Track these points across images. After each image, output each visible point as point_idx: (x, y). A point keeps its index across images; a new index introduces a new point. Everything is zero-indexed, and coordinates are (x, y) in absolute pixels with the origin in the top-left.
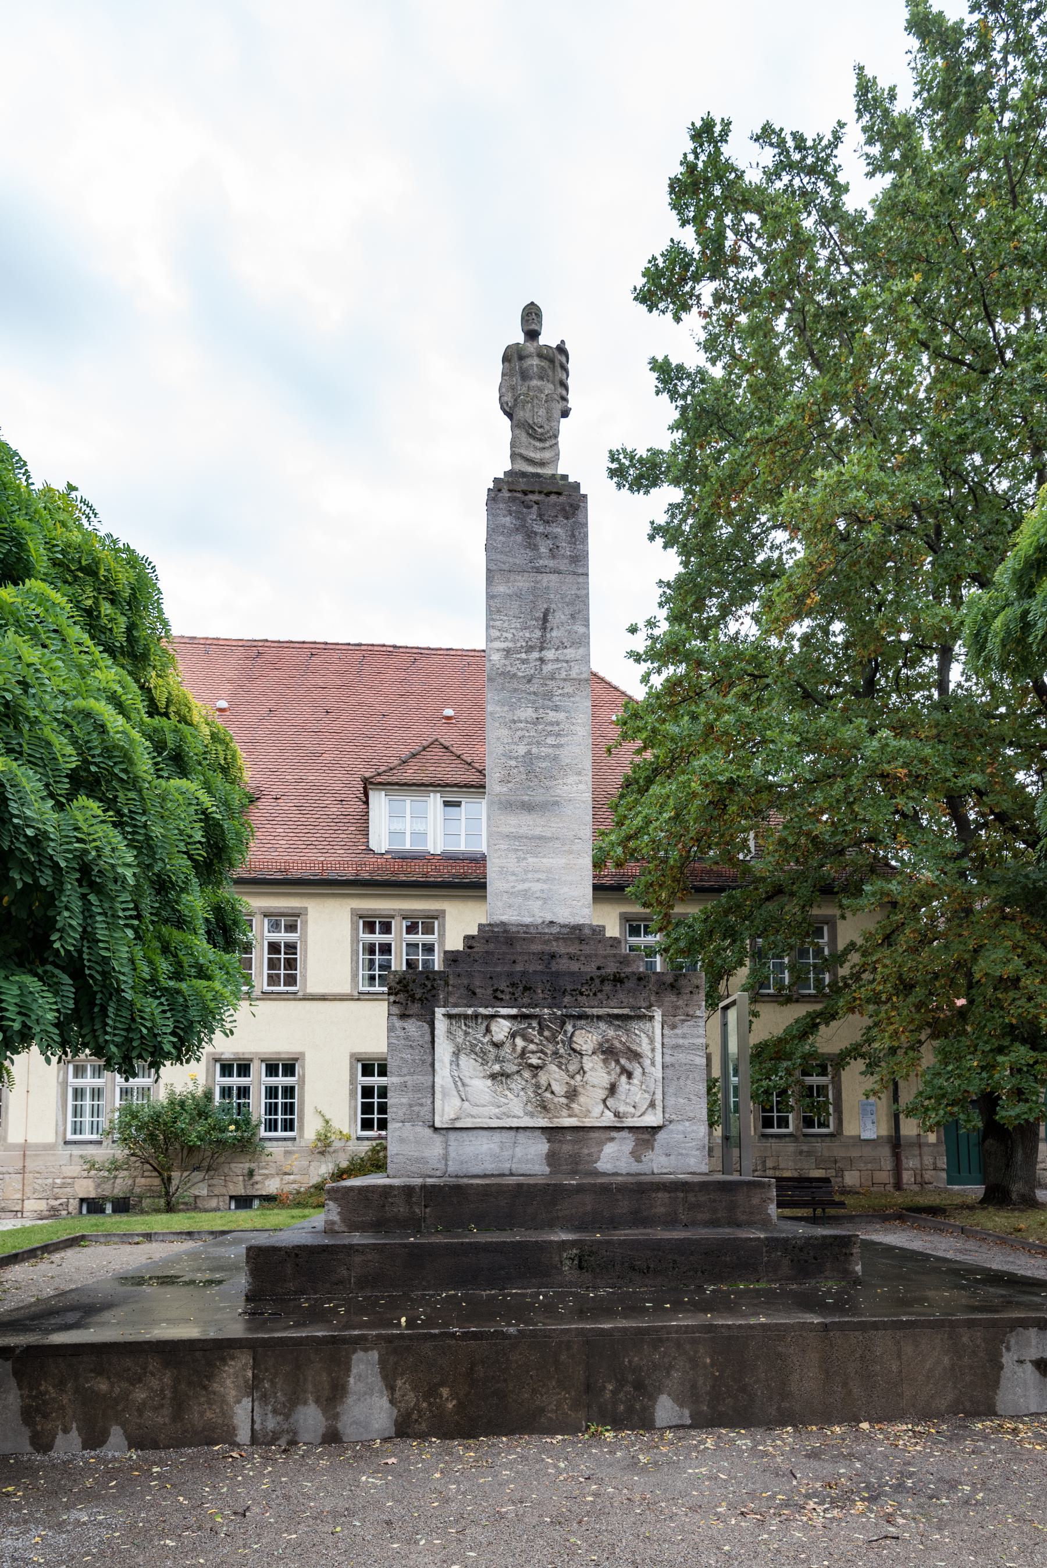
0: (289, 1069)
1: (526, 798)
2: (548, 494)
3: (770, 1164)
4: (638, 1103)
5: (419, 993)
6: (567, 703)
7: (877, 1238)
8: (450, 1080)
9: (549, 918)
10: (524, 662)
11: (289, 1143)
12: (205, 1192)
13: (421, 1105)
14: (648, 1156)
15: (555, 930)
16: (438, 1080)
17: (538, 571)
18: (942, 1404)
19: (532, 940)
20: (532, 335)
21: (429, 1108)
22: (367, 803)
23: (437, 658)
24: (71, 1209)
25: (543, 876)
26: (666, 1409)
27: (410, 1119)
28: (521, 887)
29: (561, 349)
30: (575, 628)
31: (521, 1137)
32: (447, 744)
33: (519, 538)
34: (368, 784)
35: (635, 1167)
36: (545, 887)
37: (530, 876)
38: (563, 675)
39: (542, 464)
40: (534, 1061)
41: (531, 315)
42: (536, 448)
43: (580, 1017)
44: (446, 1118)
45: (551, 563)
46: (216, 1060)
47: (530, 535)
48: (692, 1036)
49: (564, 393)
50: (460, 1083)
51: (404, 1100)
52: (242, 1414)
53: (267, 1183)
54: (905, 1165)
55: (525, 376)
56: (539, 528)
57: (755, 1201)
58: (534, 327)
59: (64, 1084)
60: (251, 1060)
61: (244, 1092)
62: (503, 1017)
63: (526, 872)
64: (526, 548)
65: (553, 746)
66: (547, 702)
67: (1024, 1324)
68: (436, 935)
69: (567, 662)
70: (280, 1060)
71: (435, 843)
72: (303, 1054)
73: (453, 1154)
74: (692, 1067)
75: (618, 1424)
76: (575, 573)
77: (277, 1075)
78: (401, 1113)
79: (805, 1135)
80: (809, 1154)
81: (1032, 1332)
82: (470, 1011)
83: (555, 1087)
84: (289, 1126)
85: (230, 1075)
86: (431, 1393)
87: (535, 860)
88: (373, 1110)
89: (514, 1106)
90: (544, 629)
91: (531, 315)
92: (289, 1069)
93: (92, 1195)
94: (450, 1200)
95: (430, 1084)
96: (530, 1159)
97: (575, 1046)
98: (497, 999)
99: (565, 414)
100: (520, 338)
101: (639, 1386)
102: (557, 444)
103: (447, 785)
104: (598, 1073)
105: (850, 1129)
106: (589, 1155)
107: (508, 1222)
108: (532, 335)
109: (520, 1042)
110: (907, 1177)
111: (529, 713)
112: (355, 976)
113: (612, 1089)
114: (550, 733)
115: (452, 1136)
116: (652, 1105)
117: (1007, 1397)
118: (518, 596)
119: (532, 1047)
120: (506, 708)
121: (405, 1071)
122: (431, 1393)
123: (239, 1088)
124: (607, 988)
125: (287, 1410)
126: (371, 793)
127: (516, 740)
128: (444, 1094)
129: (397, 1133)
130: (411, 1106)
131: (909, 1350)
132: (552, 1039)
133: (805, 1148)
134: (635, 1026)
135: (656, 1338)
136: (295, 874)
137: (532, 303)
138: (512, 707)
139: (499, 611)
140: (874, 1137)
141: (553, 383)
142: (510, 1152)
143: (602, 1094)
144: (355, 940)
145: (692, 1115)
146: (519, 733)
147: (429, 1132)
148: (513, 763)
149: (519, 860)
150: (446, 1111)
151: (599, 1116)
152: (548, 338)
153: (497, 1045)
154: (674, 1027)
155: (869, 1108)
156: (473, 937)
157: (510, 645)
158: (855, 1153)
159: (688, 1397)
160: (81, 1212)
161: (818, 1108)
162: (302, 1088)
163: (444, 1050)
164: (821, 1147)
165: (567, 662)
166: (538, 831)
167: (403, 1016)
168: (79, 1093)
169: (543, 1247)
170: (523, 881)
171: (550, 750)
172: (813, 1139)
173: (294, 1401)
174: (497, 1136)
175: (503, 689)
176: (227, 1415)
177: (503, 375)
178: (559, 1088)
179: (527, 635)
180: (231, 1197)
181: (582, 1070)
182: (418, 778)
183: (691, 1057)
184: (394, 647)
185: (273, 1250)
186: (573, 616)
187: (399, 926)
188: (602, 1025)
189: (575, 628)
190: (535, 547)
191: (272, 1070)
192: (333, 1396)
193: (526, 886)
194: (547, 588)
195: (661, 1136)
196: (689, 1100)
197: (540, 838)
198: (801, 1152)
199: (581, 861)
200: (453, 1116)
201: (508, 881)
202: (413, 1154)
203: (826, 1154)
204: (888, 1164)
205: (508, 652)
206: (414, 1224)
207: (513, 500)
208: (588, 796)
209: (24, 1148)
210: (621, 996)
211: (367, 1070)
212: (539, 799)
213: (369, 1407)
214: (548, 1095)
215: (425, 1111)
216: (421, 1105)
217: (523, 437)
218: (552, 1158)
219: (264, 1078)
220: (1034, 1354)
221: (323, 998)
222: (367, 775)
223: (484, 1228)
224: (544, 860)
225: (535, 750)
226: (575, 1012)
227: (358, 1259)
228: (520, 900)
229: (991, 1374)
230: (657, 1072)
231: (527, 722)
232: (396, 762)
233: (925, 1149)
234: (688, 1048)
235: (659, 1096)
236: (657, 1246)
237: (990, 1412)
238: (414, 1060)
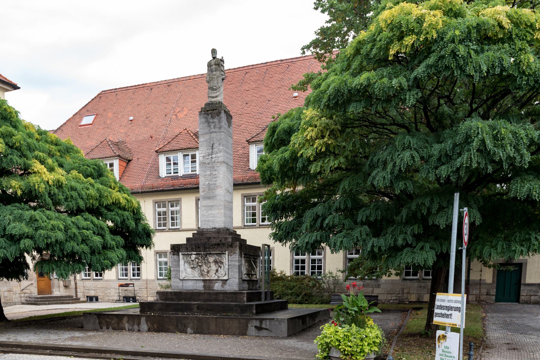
3: (405, 291)
4: (222, 274)
5: (176, 249)
9: (214, 227)
10: (208, 159)
14: (225, 286)
15: (214, 230)
17: (211, 133)
18: (237, 333)
19: (207, 234)
26: (189, 330)
27: (175, 278)
28: (207, 219)
29: (222, 60)
31: (198, 281)
33: (206, 124)
35: (222, 289)
40: (200, 264)
41: (214, 51)
43: (210, 254)
45: (214, 130)
47: (209, 123)
50: (185, 270)
52: (127, 326)
56: (211, 121)
57: (241, 297)
59: (156, 260)
67: (253, 319)
74: (235, 265)
75: (181, 332)
79: (424, 279)
81: (254, 321)
83: (205, 270)
86: (153, 325)
89: (196, 275)
90: (212, 149)
91: (214, 51)
94: (179, 295)
96: (199, 286)
98: (192, 250)
101: (185, 326)
104: (214, 267)
107: (190, 300)
108: (214, 58)
109: (197, 260)
111: (208, 173)
113: (217, 271)
114: (214, 178)
116: (226, 274)
117: (249, 332)
118: (206, 141)
122: (153, 325)
124: (216, 247)
125: (133, 325)
128: (182, 272)
131: (231, 323)
132: (204, 259)
133: (423, 285)
134: (222, 256)
135: (187, 318)
138: (205, 171)
143: (215, 272)
149: (207, 212)
150: (182, 276)
151: (213, 277)
152: (219, 56)
153: (193, 261)
154: (231, 256)
159: (193, 328)
163: (182, 262)
166: (211, 204)
167: (174, 255)
168: (160, 263)
169: (190, 304)
173: (134, 324)
174: (193, 281)
176: (125, 326)
178: (205, 271)
181: (210, 266)
184: (281, 60)
185: (143, 303)
188: (215, 256)
190: (210, 126)
192: (139, 324)
195: (228, 282)
197: (212, 206)
198: (421, 287)
202: (176, 285)
205: (204, 157)
206: (172, 300)
207: (205, 113)
209: (147, 280)
210: (219, 248)
212: (212, 195)
213: (144, 326)
217: (210, 91)
218: (204, 286)
220: (254, 325)
223: (185, 300)
226: (208, 253)
227: (158, 305)
229: (246, 328)
230: (227, 267)
232: (261, 130)
233: (483, 286)
235: (227, 272)
236: (212, 305)
237: (246, 335)
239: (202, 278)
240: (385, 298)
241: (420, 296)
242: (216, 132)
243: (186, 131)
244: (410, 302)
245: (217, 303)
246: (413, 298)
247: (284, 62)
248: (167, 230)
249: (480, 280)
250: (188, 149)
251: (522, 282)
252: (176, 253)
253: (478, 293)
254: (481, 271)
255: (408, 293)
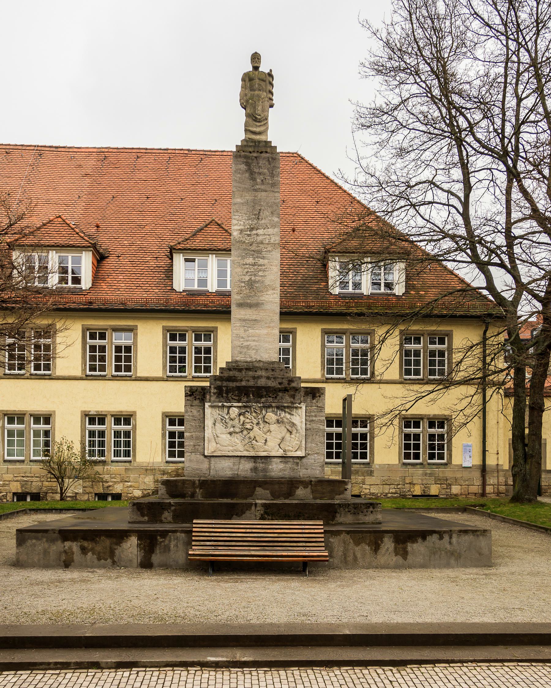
0: (127, 421)
1: (249, 301)
2: (261, 152)
6: (268, 255)
7: (427, 515)
8: (212, 434)
9: (259, 359)
10: (249, 235)
11: (128, 464)
12: (81, 491)
13: (199, 445)
16: (206, 435)
17: (256, 190)
20: (256, 68)
21: (202, 447)
22: (172, 259)
23: (215, 158)
24: (8, 498)
25: (256, 339)
27: (194, 451)
28: (246, 344)
29: (270, 75)
30: (273, 218)
32: (219, 222)
34: (172, 251)
36: (257, 344)
37: (250, 338)
38: (267, 241)
39: (260, 133)
40: (248, 426)
41: (256, 58)
42: (257, 126)
44: (210, 452)
45: (263, 187)
46: (86, 415)
48: (319, 416)
49: (271, 96)
51: (192, 443)
53: (116, 486)
54: (488, 483)
55: (252, 89)
58: (256, 65)
60: (106, 415)
61: (102, 434)
62: (235, 407)
63: (248, 337)
64: (250, 180)
65: (262, 276)
66: (259, 255)
68: (212, 342)
69: (269, 235)
70: (122, 415)
71: (212, 285)
72: (135, 412)
73: (212, 467)
76: (273, 191)
77: (121, 425)
78: (190, 449)
79: (429, 464)
80: (431, 475)
82: (220, 404)
84: (127, 454)
85: (94, 424)
87: (253, 331)
88: (175, 444)
91: (256, 58)
92: (127, 421)
93: (20, 491)
95: (203, 436)
96: (245, 469)
97: (266, 420)
99: (272, 106)
100: (250, 69)
102: (267, 123)
103: (220, 250)
105: (456, 461)
106: (272, 469)
108: (256, 68)
110: (489, 489)
112: (164, 366)
115: (212, 459)
118: (247, 203)
119: (248, 421)
120: (240, 258)
121: (192, 430)
123: (99, 431)
126: (174, 255)
127: (245, 273)
129: (189, 458)
130: (194, 446)
134: (294, 412)
136: (130, 305)
137: (256, 53)
138: (243, 258)
139: (237, 211)
140: (470, 465)
141: (266, 92)
142: (237, 467)
144: (165, 344)
145: (318, 451)
146: (246, 270)
147: (202, 457)
148: (243, 285)
150: (210, 448)
152: (264, 68)
155: (468, 448)
156: (223, 368)
157: (242, 227)
158: (458, 475)
160: (13, 501)
161: (439, 447)
162: (135, 432)
163: (209, 422)
164: (440, 472)
165: (269, 235)
166: (254, 317)
170: (247, 341)
171: (260, 278)
172: (434, 467)
174: (232, 460)
175: (239, 249)
177: (242, 87)
179: (250, 222)
180: (96, 494)
182: (202, 245)
183: (319, 425)
184: (188, 150)
186: (272, 213)
187: (190, 336)
189: (273, 218)
190: (253, 179)
191: (118, 421)
193: (248, 343)
194: (260, 199)
195: (304, 460)
196: (317, 445)
198: (426, 474)
199: (274, 331)
200: (213, 451)
201: (240, 341)
202: (192, 465)
203: (441, 475)
204: (478, 482)
208: (278, 300)
211: (172, 423)
212: (255, 302)
214: (254, 441)
215: (200, 448)
216: (199, 445)
217: (251, 121)
219: (113, 426)
221: (147, 379)
222: (172, 244)
224: (257, 331)
225: (253, 278)
228: (245, 350)
231: (250, 265)
233: (501, 473)
234: (317, 422)
238: (196, 426)
239: (252, 454)
240: (381, 491)
241: (426, 487)
242: (266, 191)
243: (60, 219)
244: (414, 496)
245: (225, 501)
246: (418, 490)
247: (193, 152)
248: (28, 375)
249: (498, 465)
250: (68, 246)
251: (543, 468)
252: (197, 402)
253: (496, 483)
254: (498, 453)
255: (410, 483)
